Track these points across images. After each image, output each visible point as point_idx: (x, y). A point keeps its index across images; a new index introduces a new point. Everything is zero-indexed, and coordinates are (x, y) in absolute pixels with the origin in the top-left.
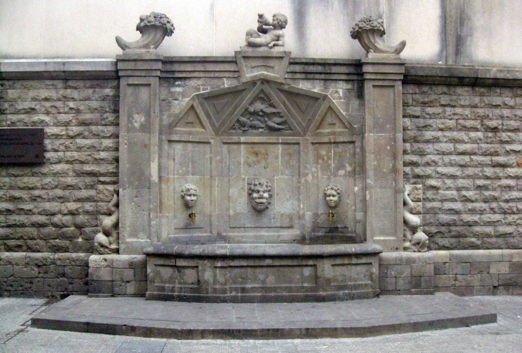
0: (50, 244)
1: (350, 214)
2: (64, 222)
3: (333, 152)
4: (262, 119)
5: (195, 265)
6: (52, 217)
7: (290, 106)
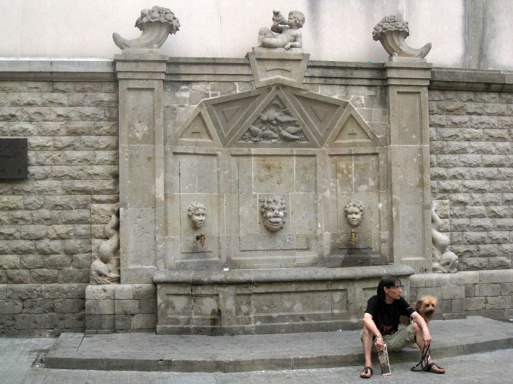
0: (36, 275)
1: (374, 232)
2: (52, 247)
3: (353, 165)
4: (275, 128)
5: (215, 293)
6: (37, 242)
7: (307, 115)
